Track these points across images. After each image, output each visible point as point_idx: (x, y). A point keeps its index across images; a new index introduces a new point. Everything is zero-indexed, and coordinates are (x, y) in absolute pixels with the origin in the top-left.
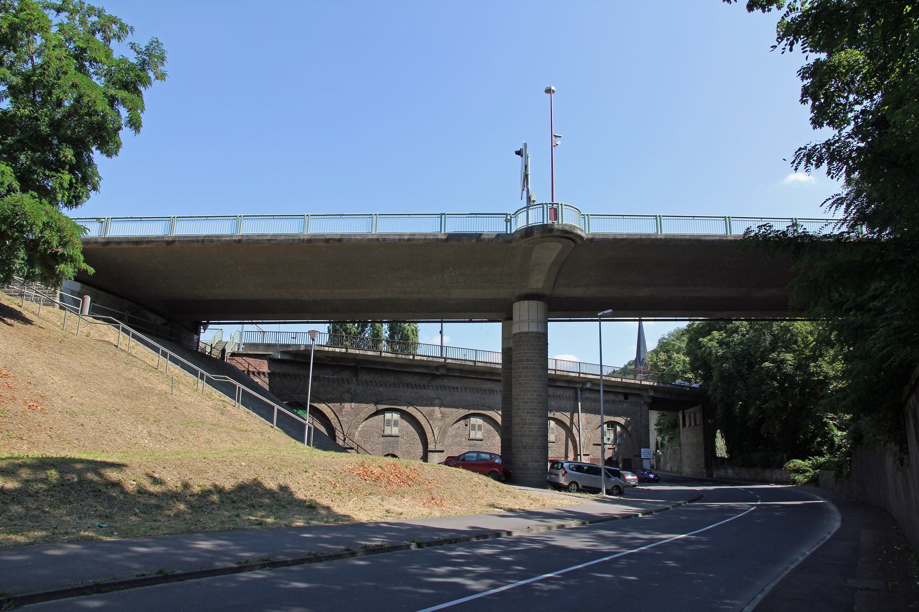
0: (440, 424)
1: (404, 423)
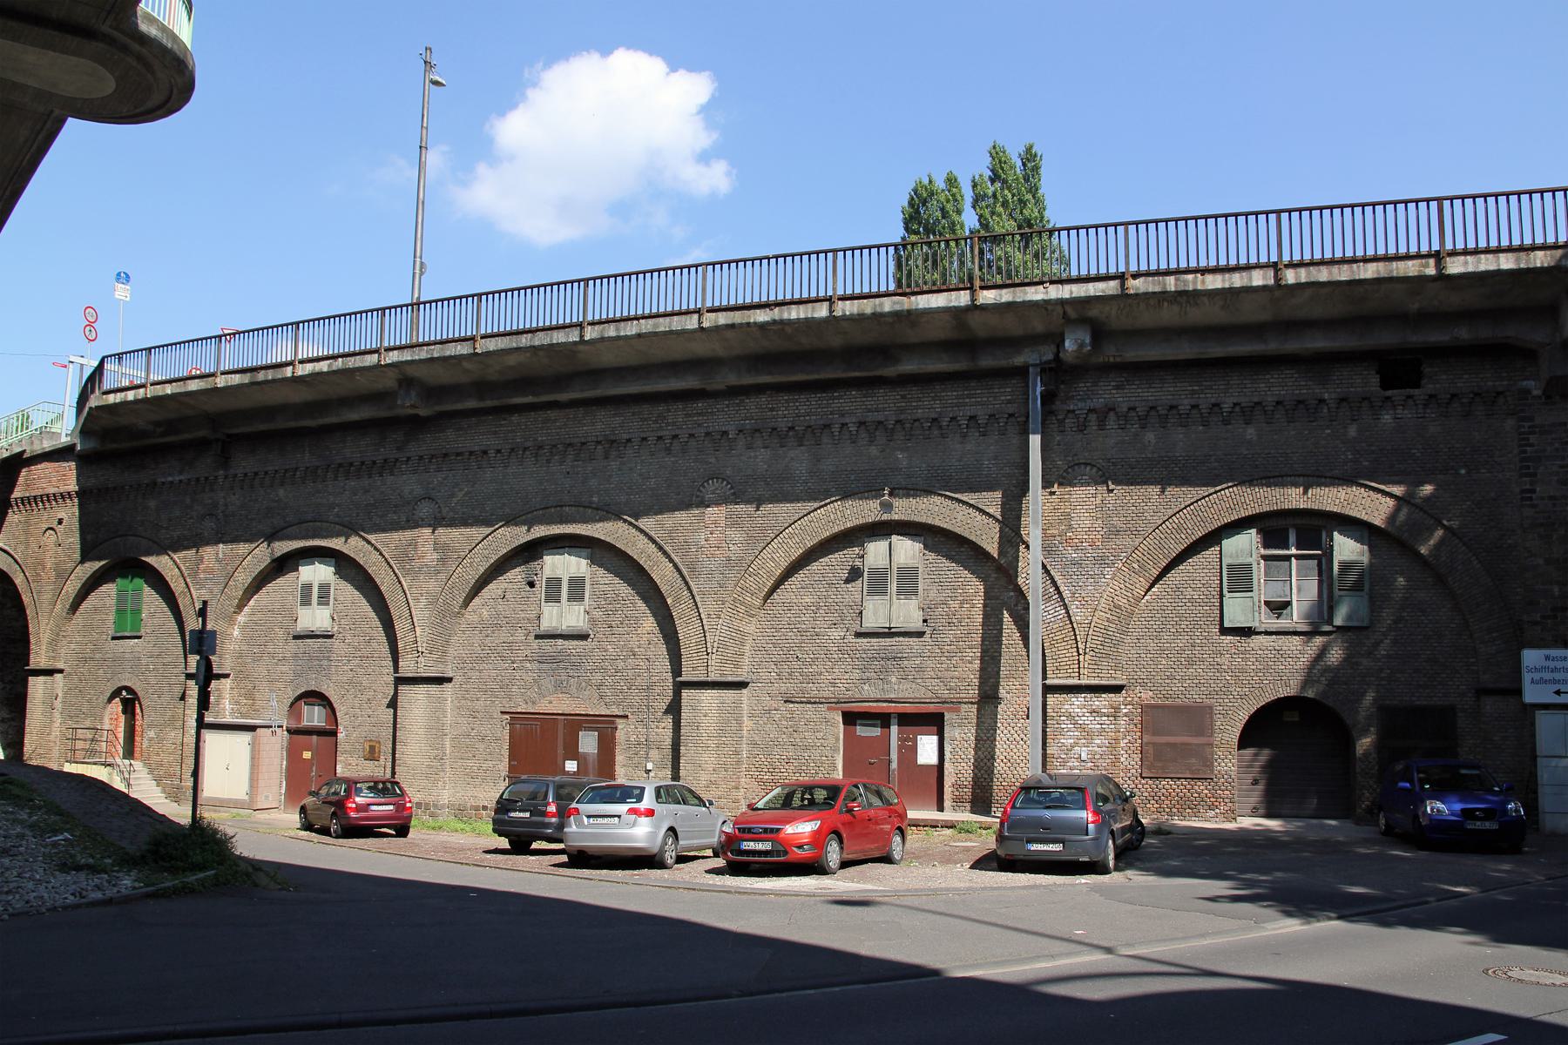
0: (432, 585)
1: (347, 593)
